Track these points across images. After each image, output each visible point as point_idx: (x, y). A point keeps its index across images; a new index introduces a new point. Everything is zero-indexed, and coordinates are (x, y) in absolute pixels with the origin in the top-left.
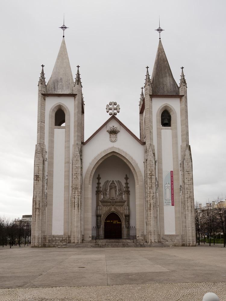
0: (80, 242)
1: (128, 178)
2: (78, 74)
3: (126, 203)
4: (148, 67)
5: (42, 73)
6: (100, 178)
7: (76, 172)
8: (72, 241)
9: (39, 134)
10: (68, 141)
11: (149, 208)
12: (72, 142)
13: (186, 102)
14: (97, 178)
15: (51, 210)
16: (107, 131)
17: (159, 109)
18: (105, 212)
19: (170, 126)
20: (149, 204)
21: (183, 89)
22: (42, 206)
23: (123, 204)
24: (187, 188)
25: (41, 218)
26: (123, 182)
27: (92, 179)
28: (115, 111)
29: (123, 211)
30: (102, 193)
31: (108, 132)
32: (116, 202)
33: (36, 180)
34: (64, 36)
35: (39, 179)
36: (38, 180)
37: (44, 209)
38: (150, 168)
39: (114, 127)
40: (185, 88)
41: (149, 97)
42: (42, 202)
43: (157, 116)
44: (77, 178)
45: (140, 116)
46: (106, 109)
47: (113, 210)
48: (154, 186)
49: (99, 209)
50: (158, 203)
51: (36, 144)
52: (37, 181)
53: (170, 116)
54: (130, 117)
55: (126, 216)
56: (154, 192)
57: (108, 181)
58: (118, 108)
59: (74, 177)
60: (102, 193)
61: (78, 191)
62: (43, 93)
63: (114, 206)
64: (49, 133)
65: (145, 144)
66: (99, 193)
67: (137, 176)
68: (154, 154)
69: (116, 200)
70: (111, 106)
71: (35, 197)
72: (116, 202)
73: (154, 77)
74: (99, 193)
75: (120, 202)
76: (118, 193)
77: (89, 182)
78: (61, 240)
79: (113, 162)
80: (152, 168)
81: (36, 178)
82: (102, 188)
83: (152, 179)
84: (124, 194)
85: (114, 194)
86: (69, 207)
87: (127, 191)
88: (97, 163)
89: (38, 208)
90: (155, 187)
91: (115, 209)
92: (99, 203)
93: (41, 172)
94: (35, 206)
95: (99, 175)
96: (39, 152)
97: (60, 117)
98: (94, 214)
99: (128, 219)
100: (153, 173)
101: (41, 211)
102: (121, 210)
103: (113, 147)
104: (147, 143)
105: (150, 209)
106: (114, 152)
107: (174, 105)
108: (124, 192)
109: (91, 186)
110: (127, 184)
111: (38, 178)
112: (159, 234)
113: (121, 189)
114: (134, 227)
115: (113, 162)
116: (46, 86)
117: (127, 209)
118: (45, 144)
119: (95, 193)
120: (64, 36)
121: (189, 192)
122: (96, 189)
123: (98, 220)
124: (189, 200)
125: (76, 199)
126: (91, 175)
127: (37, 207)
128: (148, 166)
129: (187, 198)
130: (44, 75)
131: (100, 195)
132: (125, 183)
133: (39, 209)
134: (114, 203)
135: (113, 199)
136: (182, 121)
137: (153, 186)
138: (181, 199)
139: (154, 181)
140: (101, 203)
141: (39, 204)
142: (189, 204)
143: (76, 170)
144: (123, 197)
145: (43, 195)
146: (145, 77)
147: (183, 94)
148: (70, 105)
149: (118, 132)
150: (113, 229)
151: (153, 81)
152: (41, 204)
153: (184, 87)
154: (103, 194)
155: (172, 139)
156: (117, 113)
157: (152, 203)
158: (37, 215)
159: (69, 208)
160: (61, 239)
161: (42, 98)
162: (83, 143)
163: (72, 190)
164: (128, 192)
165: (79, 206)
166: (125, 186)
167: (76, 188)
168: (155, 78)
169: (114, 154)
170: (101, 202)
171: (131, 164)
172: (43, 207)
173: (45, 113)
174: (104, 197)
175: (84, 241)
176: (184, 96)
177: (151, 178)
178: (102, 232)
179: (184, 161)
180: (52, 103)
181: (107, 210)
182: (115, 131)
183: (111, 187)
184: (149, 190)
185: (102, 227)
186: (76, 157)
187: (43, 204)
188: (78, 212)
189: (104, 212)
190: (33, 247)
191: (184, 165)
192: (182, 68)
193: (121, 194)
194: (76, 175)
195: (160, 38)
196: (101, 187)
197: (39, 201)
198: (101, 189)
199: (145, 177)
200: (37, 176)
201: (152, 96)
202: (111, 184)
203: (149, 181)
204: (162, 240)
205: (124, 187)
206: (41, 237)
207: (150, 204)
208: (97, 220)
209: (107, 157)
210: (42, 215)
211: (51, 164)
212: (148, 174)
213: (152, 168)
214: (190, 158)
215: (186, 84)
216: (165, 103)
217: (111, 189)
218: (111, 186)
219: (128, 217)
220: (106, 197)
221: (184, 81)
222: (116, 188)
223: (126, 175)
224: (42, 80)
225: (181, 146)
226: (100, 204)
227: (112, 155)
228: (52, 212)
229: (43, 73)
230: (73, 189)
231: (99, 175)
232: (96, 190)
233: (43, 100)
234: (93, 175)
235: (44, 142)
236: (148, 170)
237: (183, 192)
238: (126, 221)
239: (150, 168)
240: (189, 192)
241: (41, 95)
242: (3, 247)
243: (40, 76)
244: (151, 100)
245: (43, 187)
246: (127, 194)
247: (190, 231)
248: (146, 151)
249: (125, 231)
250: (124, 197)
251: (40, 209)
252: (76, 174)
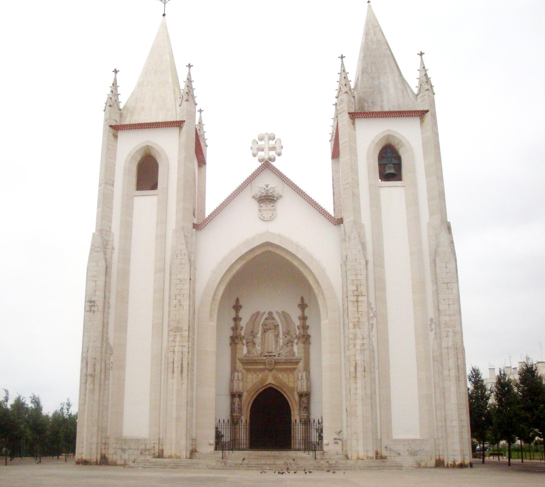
1: (306, 306)
2: (189, 80)
3: (301, 365)
4: (342, 56)
5: (113, 84)
6: (241, 307)
7: (179, 290)
9: (100, 209)
10: (162, 222)
11: (353, 375)
13: (435, 124)
14: (234, 307)
15: (121, 380)
17: (372, 142)
18: (251, 386)
21: (426, 97)
22: (101, 371)
23: (295, 366)
24: (446, 324)
25: (96, 398)
26: (295, 314)
28: (272, 153)
29: (294, 382)
30: (244, 341)
31: (256, 198)
33: (90, 311)
35: (95, 309)
36: (94, 311)
39: (269, 187)
40: (431, 94)
42: (101, 366)
44: (180, 305)
45: (332, 164)
46: (251, 149)
47: (270, 380)
48: (364, 319)
49: (236, 378)
51: (94, 232)
52: (92, 312)
53: (399, 158)
54: (310, 169)
55: (301, 395)
57: (258, 314)
58: (277, 146)
59: (175, 302)
60: (244, 341)
61: (182, 336)
62: (114, 123)
63: (274, 370)
65: (342, 223)
66: (236, 340)
67: (324, 299)
68: (363, 244)
69: (276, 358)
71: (85, 350)
72: (276, 363)
73: (358, 79)
74: (236, 340)
75: (286, 362)
76: (281, 342)
77: (211, 316)
78: (142, 450)
79: (267, 268)
80: (359, 277)
81: (91, 305)
82: (244, 330)
83: (360, 303)
84: (297, 344)
85: (274, 343)
87: (304, 336)
88: (229, 270)
89: (91, 376)
90: (367, 323)
91: (275, 378)
94: (84, 370)
95: (237, 300)
96: (97, 250)
97: (147, 173)
99: (305, 402)
100: (363, 289)
101: (97, 381)
102: (290, 383)
104: (345, 221)
105: (356, 377)
106: (267, 244)
107: (408, 133)
108: (296, 337)
109: (215, 324)
110: (303, 318)
111: (94, 306)
112: (379, 438)
113: (289, 331)
114: (316, 421)
115: (267, 268)
118: (112, 230)
119: (228, 341)
121: (451, 334)
122: (229, 333)
123: (234, 404)
124: (452, 353)
125: (176, 354)
126: (214, 299)
127: (90, 371)
128: (349, 273)
129: (448, 348)
130: (116, 90)
131: (239, 346)
132: (299, 318)
134: (273, 363)
135: (270, 356)
137: (362, 320)
138: (433, 350)
140: (241, 365)
142: (452, 363)
145: (102, 345)
146: (338, 78)
147: (425, 109)
148: (408, 133)
149: (278, 199)
151: (356, 85)
152: (98, 367)
153: (427, 92)
154: (247, 343)
156: (277, 157)
157: (359, 363)
160: (143, 447)
161: (111, 134)
163: (168, 334)
165: (185, 370)
166: (299, 325)
167: (178, 329)
168: (360, 78)
172: (103, 372)
173: (114, 165)
174: (249, 352)
175: (197, 454)
176: (428, 111)
177: (357, 301)
178: (243, 435)
179: (437, 259)
180: (130, 145)
181: (255, 380)
182: (269, 196)
183: (264, 327)
184: (352, 331)
185: (244, 421)
186: (179, 257)
187: (103, 365)
188: (182, 384)
189: (250, 385)
190: (78, 463)
191: (438, 269)
192: (421, 54)
193: (289, 343)
194: (178, 298)
197: (95, 358)
198: (243, 333)
199: (343, 300)
200: (91, 302)
201: (353, 116)
202: (266, 319)
205: (298, 327)
206: (96, 442)
207: (356, 364)
208: (232, 403)
209: (252, 256)
212: (350, 293)
213: (359, 277)
214: (450, 250)
215: (432, 87)
217: (265, 331)
218: (266, 325)
219: (305, 397)
220: (254, 351)
221: (425, 81)
222: (279, 330)
223: (302, 299)
224: (113, 98)
226: (239, 366)
230: (171, 330)
231: (237, 300)
232: (231, 335)
233: (112, 138)
234: (219, 297)
235: (110, 228)
237: (436, 333)
238: (300, 406)
239: (354, 277)
240: (451, 334)
241: (108, 127)
244: (354, 124)
245: (103, 326)
246: (304, 343)
247: (456, 430)
248: (344, 239)
249: (298, 431)
250: (297, 349)
251: (96, 377)
252: (179, 295)
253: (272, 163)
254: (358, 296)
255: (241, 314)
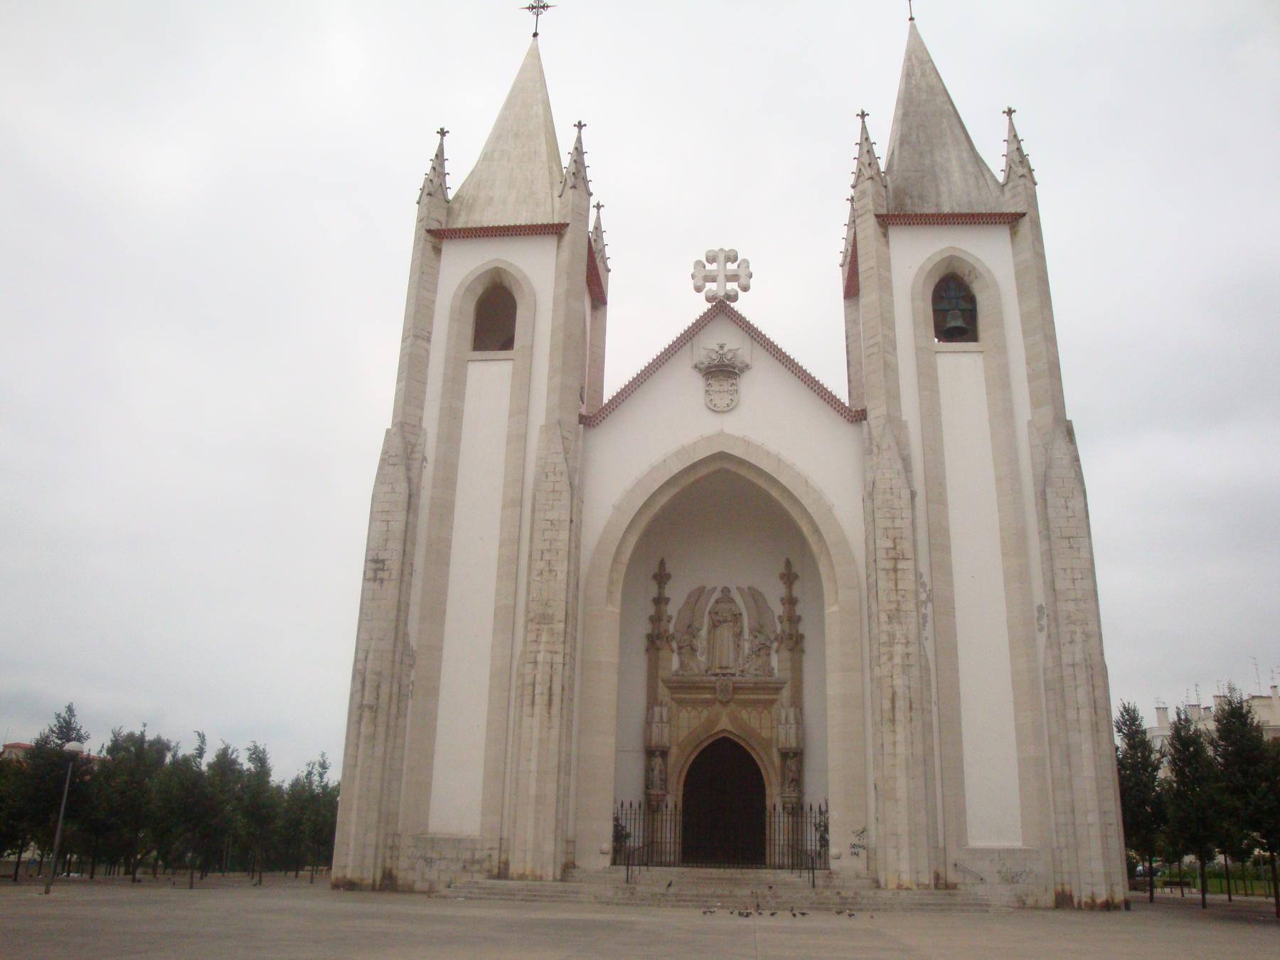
0: (551, 873)
1: (796, 577)
3: (786, 693)
6: (668, 576)
8: (514, 868)
9: (403, 384)
10: (520, 410)
11: (888, 715)
12: (539, 414)
14: (655, 577)
16: (696, 367)
17: (921, 268)
19: (974, 338)
20: (888, 693)
21: (1020, 189)
22: (390, 698)
24: (1069, 617)
26: (774, 594)
27: (621, 579)
28: (732, 286)
29: (772, 728)
30: (674, 645)
31: (700, 370)
32: (741, 688)
33: (375, 580)
34: (535, 35)
35: (385, 575)
36: (382, 580)
37: (398, 708)
38: (888, 524)
39: (726, 349)
40: (1030, 185)
41: (872, 221)
43: (913, 299)
44: (550, 571)
46: (693, 276)
47: (724, 724)
48: (909, 606)
49: (657, 718)
50: (934, 690)
53: (972, 300)
54: (801, 308)
55: (785, 755)
56: (912, 637)
57: (701, 590)
58: (742, 273)
59: (540, 565)
60: (674, 645)
62: (435, 226)
63: (732, 705)
64: (445, 381)
66: (658, 642)
69: (737, 678)
70: (711, 267)
71: (361, 656)
72: (736, 689)
74: (658, 642)
75: (757, 688)
77: (610, 593)
79: (722, 502)
80: (898, 523)
81: (376, 567)
82: (673, 621)
83: (899, 573)
86: (513, 703)
88: (647, 504)
89: (371, 708)
90: (915, 614)
91: (734, 719)
92: (668, 690)
93: (395, 546)
95: (662, 564)
97: (494, 318)
98: (635, 743)
99: (794, 768)
100: (906, 546)
101: (382, 719)
102: (764, 730)
103: (721, 434)
106: (721, 456)
107: (989, 255)
108: (776, 639)
110: (790, 601)
111: (383, 570)
114: (815, 808)
115: (722, 502)
116: (448, 202)
117: (792, 720)
118: (424, 425)
119: (642, 644)
120: (535, 35)
121: (1078, 637)
122: (644, 628)
129: (1073, 666)
130: (442, 166)
131: (664, 654)
132: (782, 600)
133: (374, 709)
135: (724, 675)
136: (1025, 318)
137: (903, 607)
139: (907, 583)
141: (378, 686)
142: (1082, 695)
143: (549, 535)
144: (775, 661)
145: (395, 645)
146: (855, 151)
147: (1019, 210)
148: (989, 255)
150: (723, 808)
151: (889, 166)
152: (385, 690)
153: (1022, 181)
154: (680, 648)
155: (988, 393)
156: (741, 294)
157: (900, 691)
158: (362, 739)
159: (512, 709)
160: (468, 855)
161: (429, 246)
162: (587, 421)
164: (797, 643)
167: (545, 619)
169: (726, 465)
170: (669, 688)
171: (804, 511)
173: (433, 302)
176: (1024, 215)
177: (895, 570)
178: (670, 834)
179: (1048, 490)
180: (463, 266)
182: (726, 366)
184: (885, 627)
186: (552, 478)
187: (395, 686)
190: (336, 886)
191: (1050, 510)
192: (1010, 112)
193: (762, 650)
194: (547, 556)
195: (911, 19)
196: (670, 618)
197: (379, 674)
198: (671, 629)
199: (867, 567)
200: (376, 561)
201: (885, 221)
202: (717, 602)
203: (884, 583)
204: (952, 877)
207: (894, 694)
208: (649, 770)
209: (691, 479)
210: (386, 740)
211: (445, 511)
212: (881, 554)
216: (947, 245)
217: (714, 626)
218: (716, 613)
219: (794, 757)
221: (1018, 160)
222: (742, 622)
223: (788, 563)
225: (1030, 424)
227: (719, 471)
228: (435, 729)
229: (440, 156)
230: (532, 620)
232: (649, 631)
233: (430, 253)
236: (879, 532)
237: (1049, 636)
238: (783, 776)
239: (888, 524)
240: (1078, 637)
241: (423, 232)
242: (47, 892)
243: (427, 167)
244: (885, 235)
245: (399, 610)
246: (791, 650)
249: (779, 828)
250: (777, 662)
252: (549, 550)
253: (732, 305)
254: (896, 559)
255: (669, 591)
